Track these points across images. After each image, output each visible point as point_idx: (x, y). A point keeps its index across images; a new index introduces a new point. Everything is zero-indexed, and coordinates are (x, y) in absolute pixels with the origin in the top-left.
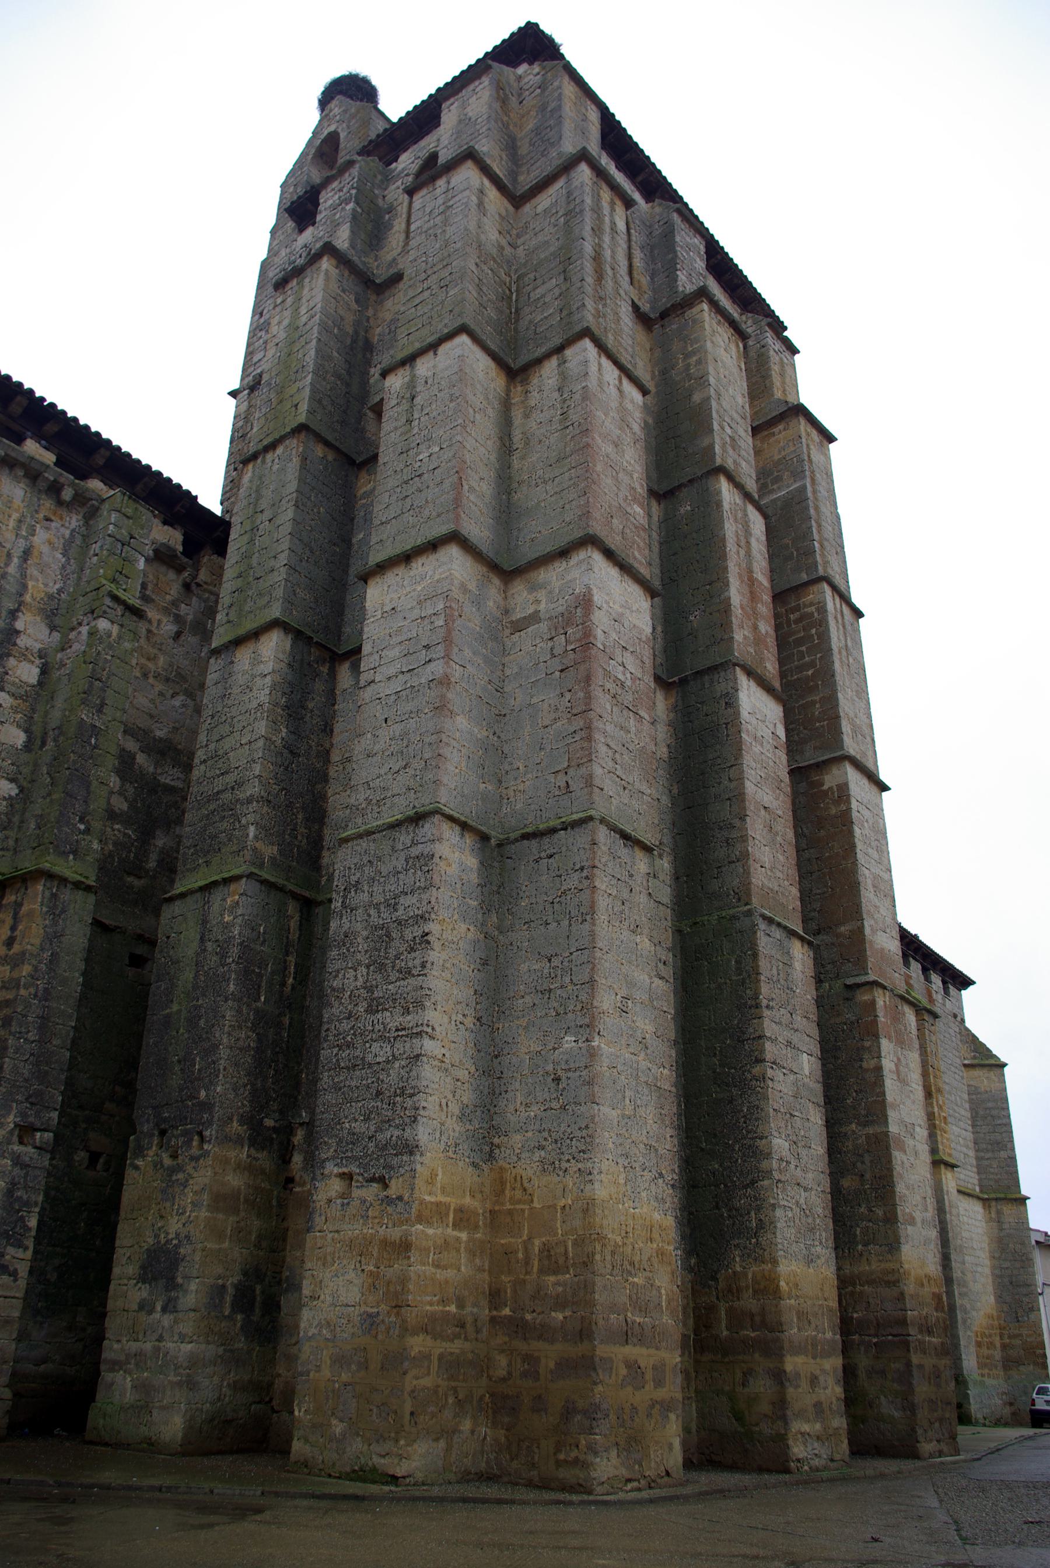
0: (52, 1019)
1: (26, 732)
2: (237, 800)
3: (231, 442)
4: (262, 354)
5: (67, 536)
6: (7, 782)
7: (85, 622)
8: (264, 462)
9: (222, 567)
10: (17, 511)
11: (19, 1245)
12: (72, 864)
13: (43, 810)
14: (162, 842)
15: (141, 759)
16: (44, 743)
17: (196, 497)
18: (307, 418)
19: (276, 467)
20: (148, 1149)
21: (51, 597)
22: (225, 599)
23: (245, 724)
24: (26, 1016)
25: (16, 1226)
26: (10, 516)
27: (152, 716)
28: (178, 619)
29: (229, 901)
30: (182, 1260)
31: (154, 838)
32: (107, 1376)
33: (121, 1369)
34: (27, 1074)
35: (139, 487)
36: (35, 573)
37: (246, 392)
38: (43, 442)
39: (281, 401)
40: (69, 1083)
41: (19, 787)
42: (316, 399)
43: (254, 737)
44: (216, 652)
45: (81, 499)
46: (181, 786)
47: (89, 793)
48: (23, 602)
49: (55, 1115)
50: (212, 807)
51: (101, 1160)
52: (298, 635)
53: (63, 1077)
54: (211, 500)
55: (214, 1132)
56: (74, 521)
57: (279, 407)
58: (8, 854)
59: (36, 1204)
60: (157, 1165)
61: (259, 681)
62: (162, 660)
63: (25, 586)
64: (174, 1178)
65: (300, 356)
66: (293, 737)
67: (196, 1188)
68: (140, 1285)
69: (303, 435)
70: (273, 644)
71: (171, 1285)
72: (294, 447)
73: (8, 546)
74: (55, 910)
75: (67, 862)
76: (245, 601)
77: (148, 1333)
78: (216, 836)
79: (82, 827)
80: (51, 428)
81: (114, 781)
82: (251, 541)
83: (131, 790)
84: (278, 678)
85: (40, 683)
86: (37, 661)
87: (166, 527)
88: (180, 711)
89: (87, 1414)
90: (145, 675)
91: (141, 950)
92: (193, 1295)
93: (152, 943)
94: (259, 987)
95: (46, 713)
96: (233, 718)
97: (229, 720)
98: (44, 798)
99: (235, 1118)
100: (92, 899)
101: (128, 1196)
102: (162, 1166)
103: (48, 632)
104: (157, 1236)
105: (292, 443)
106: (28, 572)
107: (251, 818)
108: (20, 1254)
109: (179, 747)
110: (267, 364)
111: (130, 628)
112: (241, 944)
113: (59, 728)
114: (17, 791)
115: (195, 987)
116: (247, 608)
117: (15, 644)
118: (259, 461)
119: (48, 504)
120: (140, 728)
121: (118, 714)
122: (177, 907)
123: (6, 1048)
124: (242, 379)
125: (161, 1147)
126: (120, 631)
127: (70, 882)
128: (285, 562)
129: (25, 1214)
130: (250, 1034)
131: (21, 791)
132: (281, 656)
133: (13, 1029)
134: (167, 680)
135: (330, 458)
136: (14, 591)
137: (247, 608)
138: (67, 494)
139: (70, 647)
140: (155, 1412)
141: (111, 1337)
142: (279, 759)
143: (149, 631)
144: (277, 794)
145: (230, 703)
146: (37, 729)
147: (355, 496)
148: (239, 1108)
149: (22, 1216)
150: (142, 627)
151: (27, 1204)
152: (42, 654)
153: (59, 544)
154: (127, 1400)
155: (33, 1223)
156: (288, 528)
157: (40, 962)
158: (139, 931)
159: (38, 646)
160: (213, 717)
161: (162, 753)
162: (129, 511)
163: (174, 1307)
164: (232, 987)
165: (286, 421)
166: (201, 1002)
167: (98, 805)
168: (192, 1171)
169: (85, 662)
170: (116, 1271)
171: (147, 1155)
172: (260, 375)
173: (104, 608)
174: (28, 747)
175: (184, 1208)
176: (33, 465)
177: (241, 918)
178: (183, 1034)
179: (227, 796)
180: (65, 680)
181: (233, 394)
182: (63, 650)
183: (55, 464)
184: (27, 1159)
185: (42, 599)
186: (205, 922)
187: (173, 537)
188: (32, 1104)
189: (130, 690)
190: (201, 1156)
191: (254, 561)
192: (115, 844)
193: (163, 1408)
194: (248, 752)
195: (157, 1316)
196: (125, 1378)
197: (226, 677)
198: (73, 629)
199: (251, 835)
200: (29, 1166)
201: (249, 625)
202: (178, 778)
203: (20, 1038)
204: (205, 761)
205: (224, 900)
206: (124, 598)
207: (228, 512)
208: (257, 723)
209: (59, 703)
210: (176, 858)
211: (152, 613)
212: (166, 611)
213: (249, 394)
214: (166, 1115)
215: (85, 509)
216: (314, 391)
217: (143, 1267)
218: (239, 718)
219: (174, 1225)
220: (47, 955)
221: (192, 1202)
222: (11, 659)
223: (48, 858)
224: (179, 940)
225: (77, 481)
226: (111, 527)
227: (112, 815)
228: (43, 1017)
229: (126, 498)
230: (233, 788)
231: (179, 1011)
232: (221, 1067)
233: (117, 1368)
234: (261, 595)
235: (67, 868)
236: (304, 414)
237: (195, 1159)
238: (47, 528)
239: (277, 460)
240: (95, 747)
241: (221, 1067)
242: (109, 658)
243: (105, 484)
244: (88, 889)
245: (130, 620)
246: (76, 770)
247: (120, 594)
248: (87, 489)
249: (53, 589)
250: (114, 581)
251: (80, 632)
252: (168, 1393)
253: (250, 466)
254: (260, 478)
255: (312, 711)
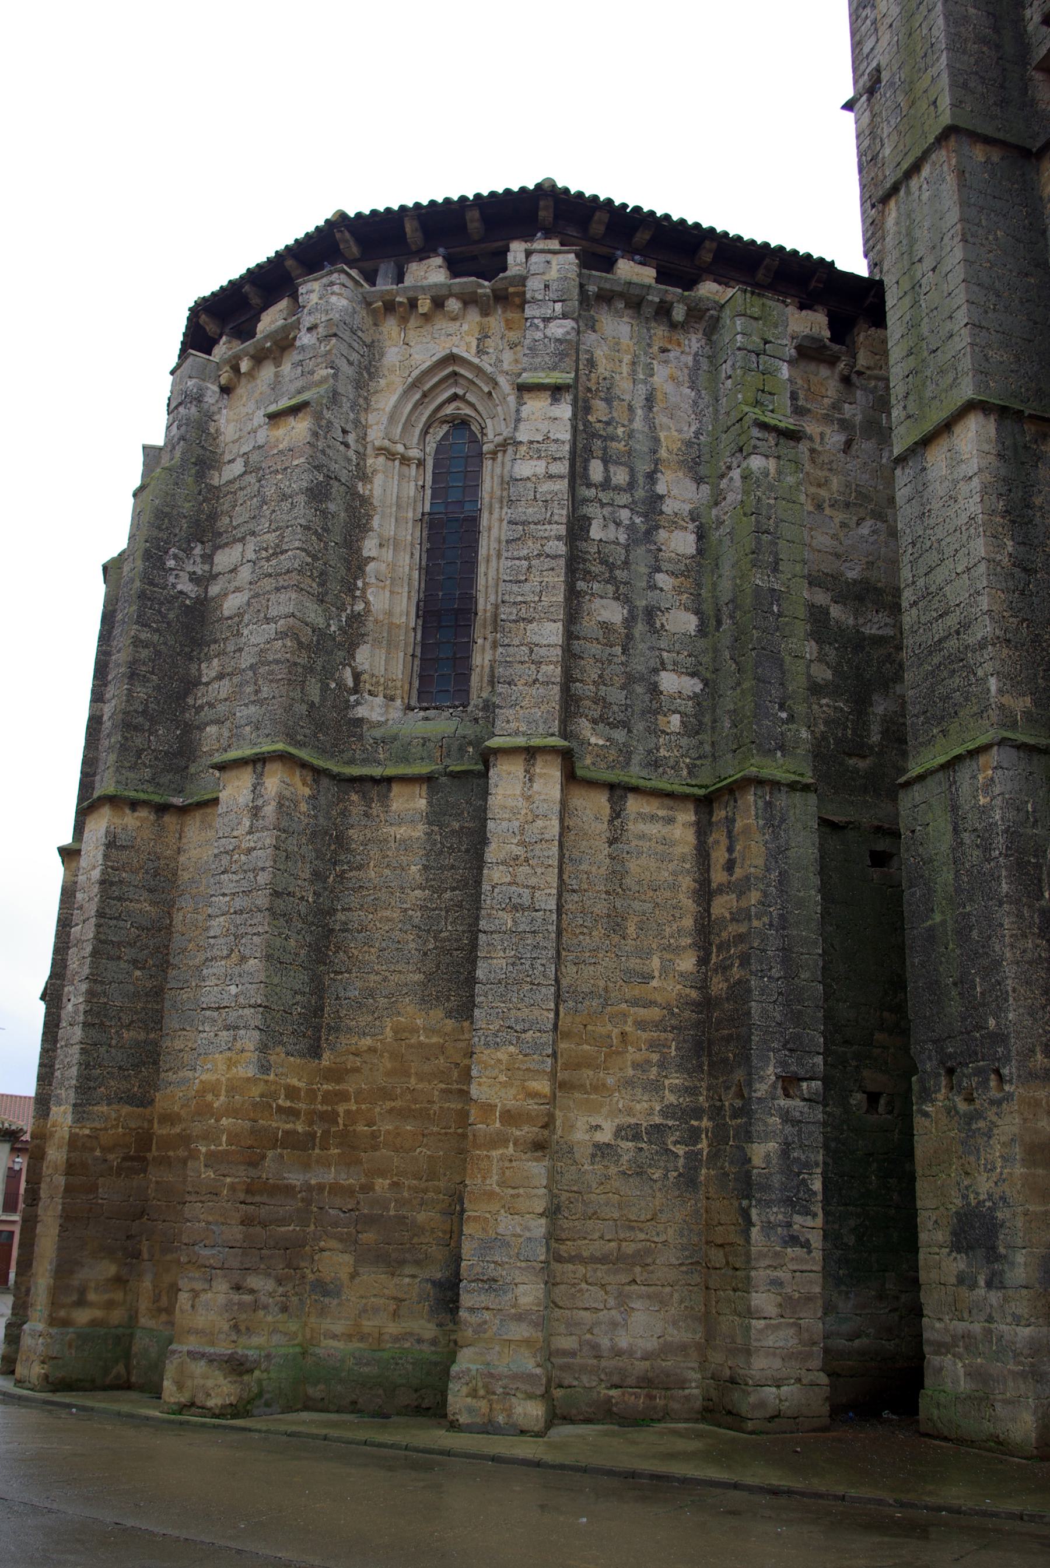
0: (796, 949)
1: (696, 614)
2: (967, 647)
3: (860, 171)
4: (873, 39)
5: (691, 364)
6: (689, 678)
7: (735, 465)
8: (908, 193)
9: (884, 342)
10: (627, 352)
11: (807, 1212)
12: (781, 762)
13: (735, 703)
14: (882, 708)
15: (836, 611)
16: (719, 623)
17: (833, 262)
18: (953, 115)
19: (926, 195)
20: (935, 1092)
21: (689, 444)
22: (898, 388)
23: (957, 546)
24: (764, 951)
25: (799, 1191)
26: (620, 361)
27: (838, 556)
28: (845, 425)
29: (980, 777)
30: (1001, 1226)
31: (871, 705)
32: (933, 1360)
33: (948, 1352)
34: (778, 1017)
35: (760, 275)
36: (665, 420)
37: (864, 98)
38: (637, 257)
39: (913, 103)
40: (828, 1018)
41: (702, 681)
42: (959, 84)
43: (972, 562)
44: (901, 460)
45: (696, 313)
46: (892, 633)
47: (783, 673)
48: (658, 459)
49: (819, 1060)
50: (936, 661)
51: (882, 1101)
52: (1002, 413)
53: (820, 1015)
54: (853, 261)
55: (1014, 1070)
56: (694, 342)
57: (912, 111)
58: (707, 762)
59: (817, 1165)
60: (951, 1111)
61: (964, 488)
62: (835, 482)
63: (657, 440)
64: (974, 1126)
65: (924, 32)
66: (1022, 549)
67: (1003, 1139)
68: (954, 1254)
69: (952, 142)
70: (972, 434)
71: (993, 1255)
72: (944, 160)
73: (627, 397)
74: (773, 822)
75: (776, 761)
76: (924, 384)
77: (974, 1312)
78: (948, 697)
79: (784, 715)
80: (642, 237)
81: (810, 649)
82: (915, 303)
83: (832, 653)
84: (987, 477)
85: (700, 552)
86: (691, 526)
87: (804, 312)
88: (871, 539)
89: (918, 1402)
90: (819, 507)
91: (882, 845)
92: (1022, 1270)
93: (896, 835)
94: (1040, 880)
95: (714, 585)
96: (939, 541)
97: (936, 545)
98: (733, 689)
99: (1038, 1049)
100: (812, 798)
101: (922, 1148)
102: (957, 1113)
103: (695, 486)
104: (965, 1197)
105: (940, 155)
106: (657, 421)
107: (988, 667)
108: (809, 1222)
109: (879, 585)
110: (883, 54)
111: (790, 457)
112: (1006, 831)
113: (732, 601)
114: (701, 686)
115: (958, 890)
116: (928, 394)
117: (662, 513)
118: (902, 193)
119: (660, 331)
120: (827, 574)
121: (798, 567)
122: (917, 793)
123: (749, 991)
124: (855, 82)
125: (952, 1088)
126: (778, 464)
127: (783, 785)
128: (966, 321)
129: (806, 1176)
130: (1038, 941)
131: (706, 685)
132: (986, 447)
133: (753, 968)
134: (847, 505)
135: (995, 158)
136: (646, 449)
137: (928, 394)
138: (679, 313)
139: (725, 499)
140: (998, 1406)
141: (930, 1314)
142: (1010, 583)
143: (812, 451)
144: (1017, 629)
145: (932, 522)
146: (708, 608)
147: (1041, 198)
148: (1041, 1036)
149: (803, 1179)
150: (803, 447)
151: (807, 1165)
152: (694, 516)
153: (683, 376)
154: (962, 1389)
155: (817, 1185)
156: (959, 273)
157: (768, 885)
158: (876, 823)
159: (688, 507)
160: (913, 544)
161: (860, 599)
162: (756, 311)
163: (1001, 1282)
164: (1005, 887)
165: (926, 128)
166: (968, 909)
167: (797, 684)
168: (995, 1118)
169: (745, 515)
170: (923, 1237)
171: (936, 1100)
172: (878, 70)
173: (753, 442)
174: (702, 631)
175: (993, 1163)
176: (632, 291)
177: (1000, 798)
178: (953, 950)
179: (952, 644)
180: (727, 541)
181: (848, 106)
182: (716, 504)
183: (658, 280)
184: (798, 1114)
185: (679, 449)
186: (955, 808)
187: (813, 323)
188: (790, 1050)
189: (806, 533)
190: (1004, 1099)
191: (925, 329)
192: (826, 723)
193: (1007, 1402)
194: (967, 582)
195: (981, 1291)
196: (955, 1364)
197: (920, 491)
198: (722, 476)
199: (993, 689)
200: (800, 1121)
201: (936, 416)
202: (886, 625)
203: (762, 977)
204: (915, 603)
205: (974, 777)
206: (773, 422)
207: (876, 265)
208: (972, 543)
209: (726, 570)
210: (904, 724)
211: (811, 428)
212: (827, 419)
213: (869, 100)
214: (951, 1050)
215: (704, 324)
216: (953, 75)
217: (954, 1233)
218: (948, 539)
219: (984, 1185)
220: (774, 875)
221: (1002, 1157)
222: (661, 531)
223: (753, 761)
224: (928, 834)
225: (686, 293)
226: (739, 337)
227: (815, 689)
228: (784, 949)
229: (748, 295)
230: (958, 633)
231: (944, 922)
232: (1009, 988)
233: (943, 1350)
234: (942, 372)
235: (777, 768)
236: (948, 111)
237: (998, 1103)
238: (665, 362)
239: (925, 186)
240: (780, 615)
241: (1009, 988)
242: (772, 502)
243: (720, 284)
244: (806, 788)
245: (787, 448)
246: (763, 648)
247: (769, 419)
248: (700, 299)
249: (689, 433)
250: (757, 403)
251: (732, 479)
252: (1011, 1384)
253: (892, 203)
254: (909, 216)
255: (1041, 508)
